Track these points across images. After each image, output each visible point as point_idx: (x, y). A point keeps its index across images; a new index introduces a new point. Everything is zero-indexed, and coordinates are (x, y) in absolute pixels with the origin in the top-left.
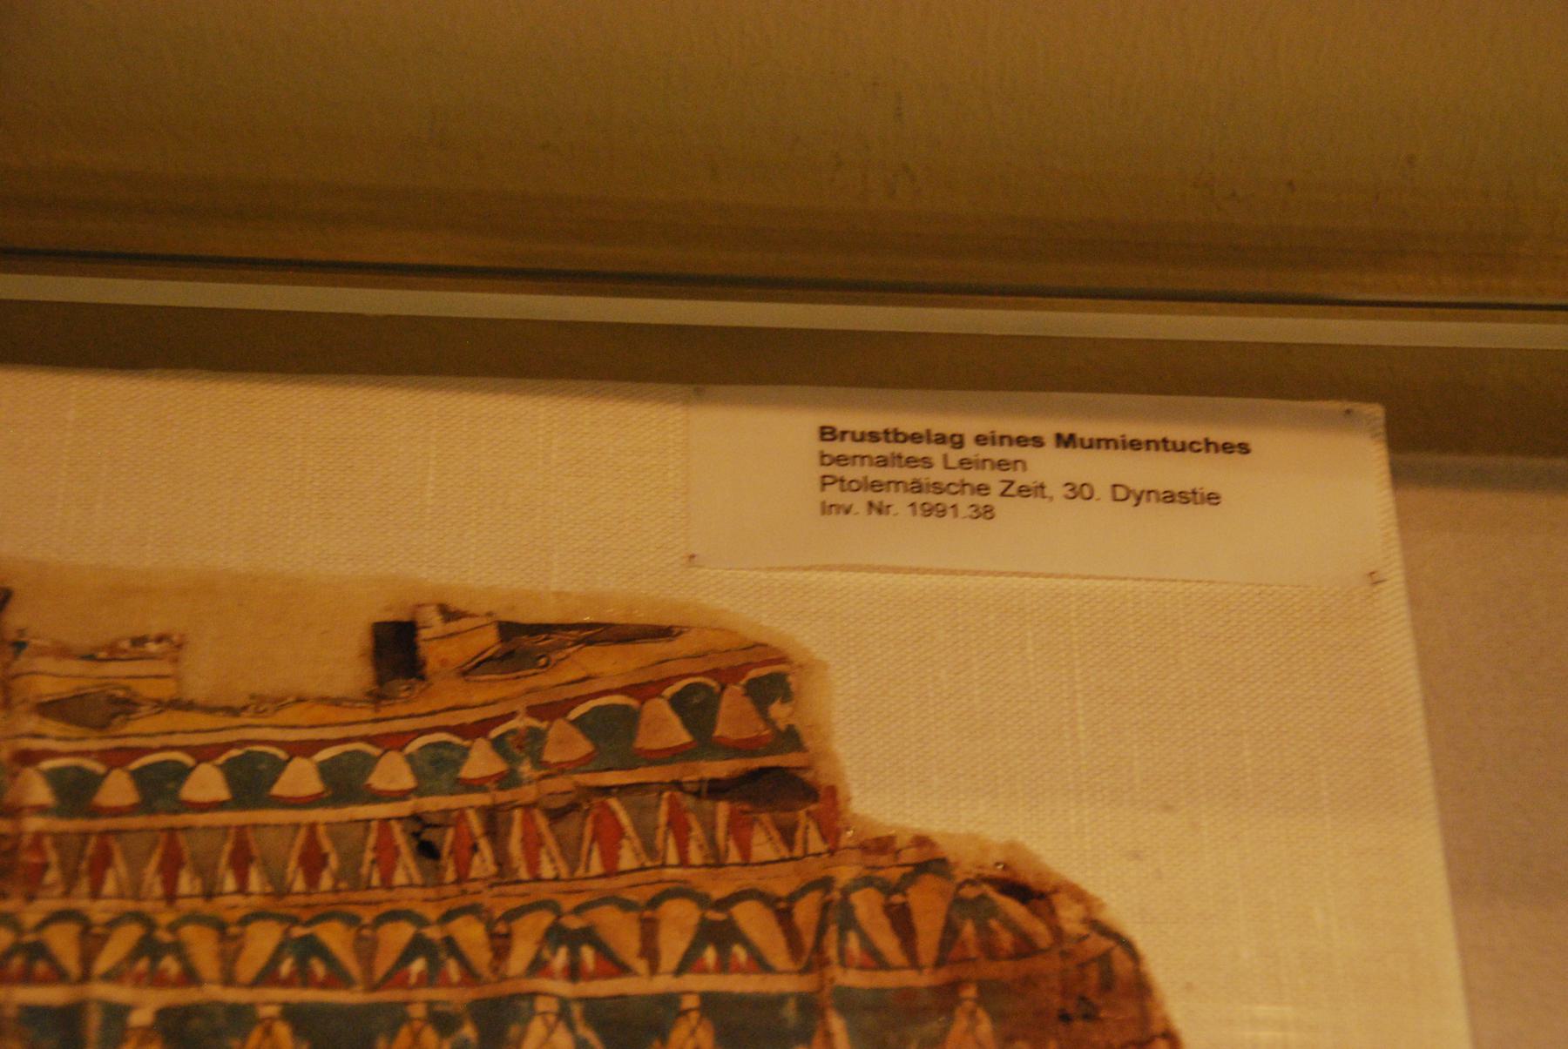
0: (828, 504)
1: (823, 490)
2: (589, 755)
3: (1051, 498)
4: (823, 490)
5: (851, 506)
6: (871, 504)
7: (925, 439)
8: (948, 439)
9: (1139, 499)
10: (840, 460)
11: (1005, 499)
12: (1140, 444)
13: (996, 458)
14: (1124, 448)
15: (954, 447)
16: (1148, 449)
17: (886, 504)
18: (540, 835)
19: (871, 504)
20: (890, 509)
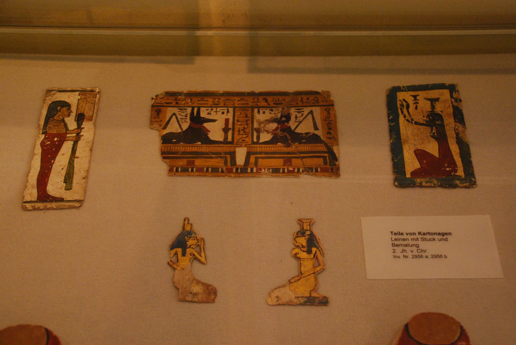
0: (395, 256)
1: (447, 238)
2: (221, 141)
3: (429, 258)
4: (447, 238)
5: (400, 256)
6: (404, 256)
7: (397, 234)
8: (441, 234)
9: (456, 100)
10: (396, 240)
11: (413, 259)
12: (447, 233)
13: (402, 238)
14: (400, 235)
15: (443, 236)
16: (449, 235)
17: (407, 256)
18: (225, 156)
19: (404, 256)
20: (426, 251)
